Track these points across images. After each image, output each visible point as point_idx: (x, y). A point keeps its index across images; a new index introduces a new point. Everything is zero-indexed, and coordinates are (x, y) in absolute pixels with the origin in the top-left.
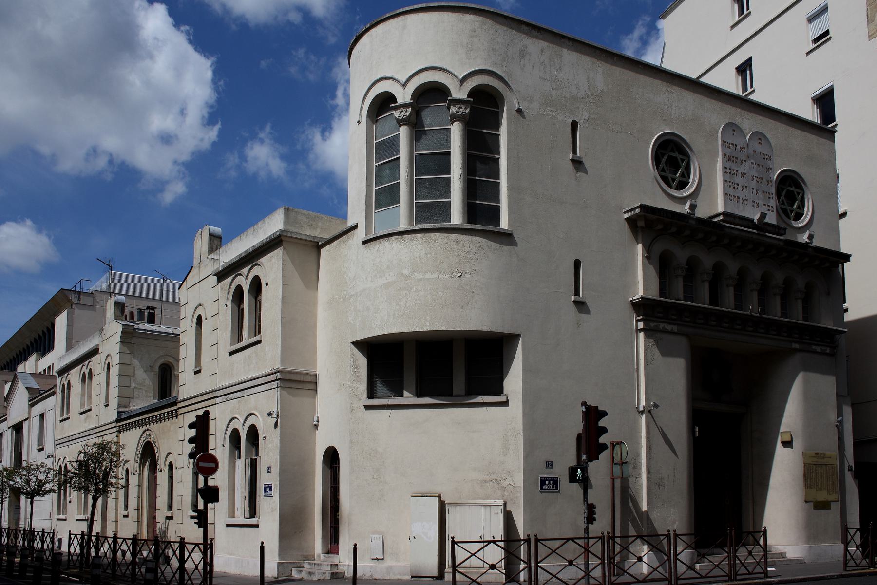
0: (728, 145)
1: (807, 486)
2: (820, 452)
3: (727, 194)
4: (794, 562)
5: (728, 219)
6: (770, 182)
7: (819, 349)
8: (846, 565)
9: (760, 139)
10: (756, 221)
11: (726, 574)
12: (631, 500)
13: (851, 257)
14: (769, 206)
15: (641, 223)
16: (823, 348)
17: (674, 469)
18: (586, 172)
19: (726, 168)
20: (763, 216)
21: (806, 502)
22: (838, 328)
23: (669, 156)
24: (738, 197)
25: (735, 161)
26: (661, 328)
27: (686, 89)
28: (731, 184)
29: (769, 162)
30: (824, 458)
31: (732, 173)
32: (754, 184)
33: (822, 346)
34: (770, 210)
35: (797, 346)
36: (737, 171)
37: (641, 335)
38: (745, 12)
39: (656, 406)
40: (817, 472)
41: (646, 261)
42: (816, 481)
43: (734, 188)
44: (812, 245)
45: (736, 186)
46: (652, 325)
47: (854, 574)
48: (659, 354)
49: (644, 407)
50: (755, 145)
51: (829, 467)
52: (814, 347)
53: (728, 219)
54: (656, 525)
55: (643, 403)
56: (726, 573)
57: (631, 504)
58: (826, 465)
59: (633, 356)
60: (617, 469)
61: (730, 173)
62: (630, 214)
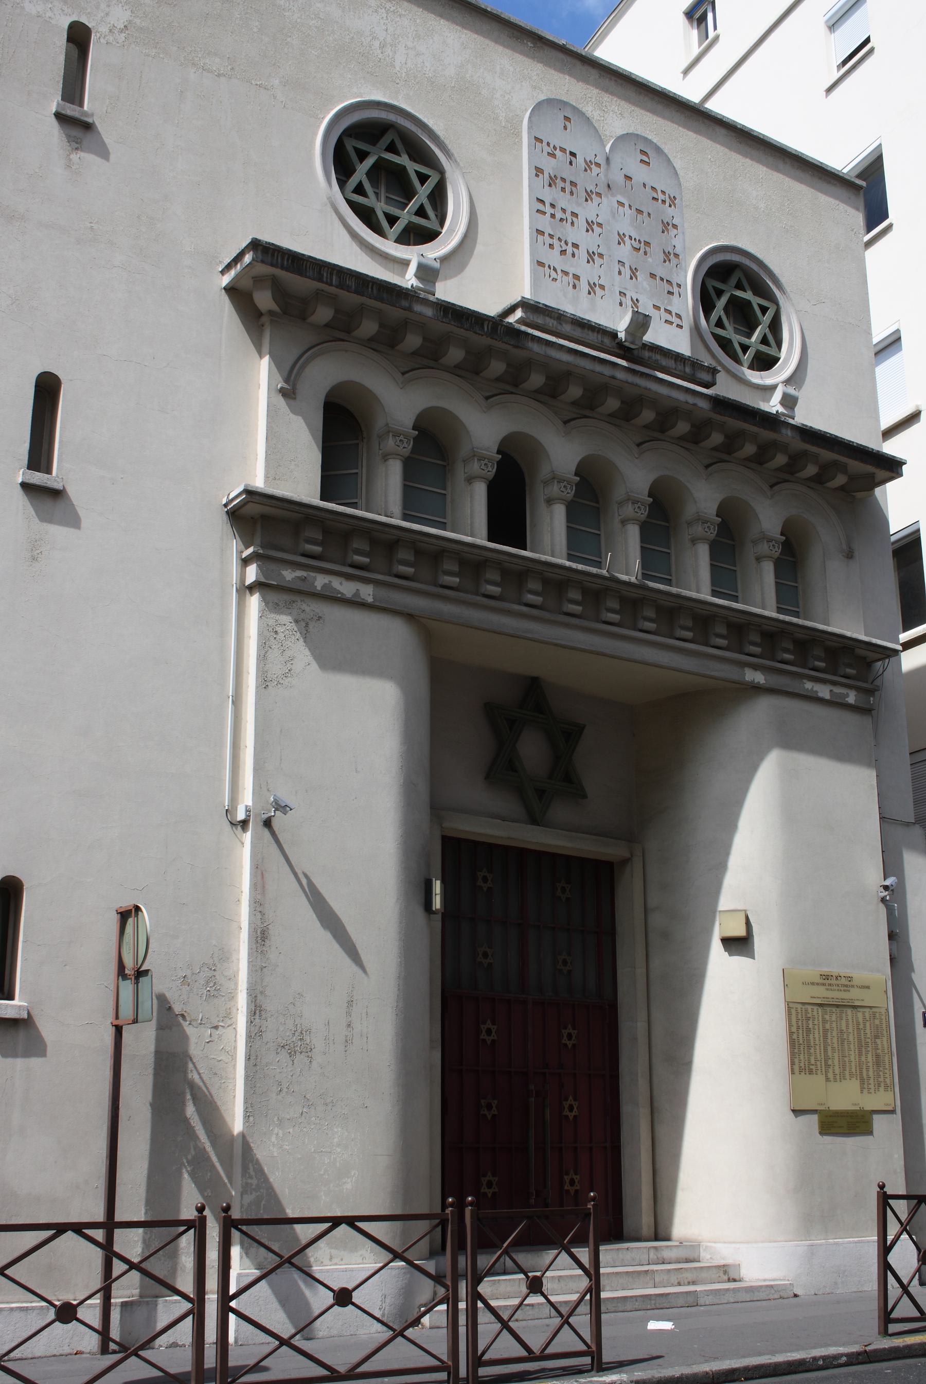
0: (547, 149)
1: (796, 1068)
2: (834, 970)
3: (541, 264)
4: (762, 1295)
5: (540, 320)
6: (672, 256)
7: (824, 691)
8: (886, 1317)
9: (643, 152)
10: (622, 335)
11: (436, 1363)
12: (192, 1095)
13: (904, 467)
14: (670, 312)
15: (264, 300)
16: (838, 690)
17: (350, 1003)
18: (103, 152)
19: (541, 201)
20: (641, 322)
21: (797, 1112)
22: (874, 641)
23: (380, 159)
24: (576, 277)
25: (568, 190)
26: (319, 588)
27: (441, 16)
28: (555, 242)
29: (671, 211)
30: (847, 987)
31: (559, 215)
32: (625, 252)
33: (834, 683)
34: (671, 323)
35: (759, 678)
36: (575, 215)
37: (254, 602)
38: (711, 34)
39: (281, 807)
40: (828, 1026)
41: (281, 401)
42: (826, 1051)
43: (563, 252)
44: (791, 421)
45: (570, 249)
46: (289, 575)
47: (909, 1347)
48: (310, 658)
49: (248, 810)
50: (630, 163)
51: (864, 1013)
52: (809, 685)
53: (540, 320)
54: (275, 1178)
55: (247, 799)
56: (484, 1353)
57: (190, 1110)
58: (854, 1007)
59: (224, 661)
60: (127, 988)
61: (553, 216)
62: (232, 273)
